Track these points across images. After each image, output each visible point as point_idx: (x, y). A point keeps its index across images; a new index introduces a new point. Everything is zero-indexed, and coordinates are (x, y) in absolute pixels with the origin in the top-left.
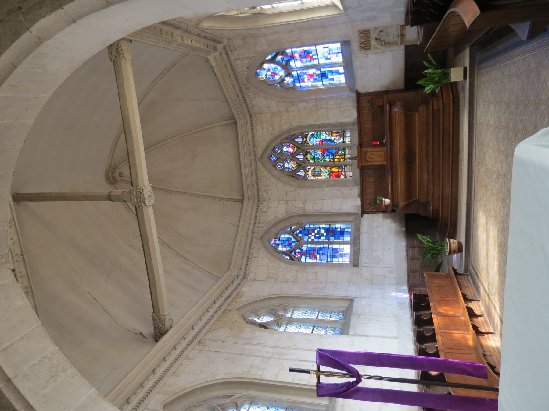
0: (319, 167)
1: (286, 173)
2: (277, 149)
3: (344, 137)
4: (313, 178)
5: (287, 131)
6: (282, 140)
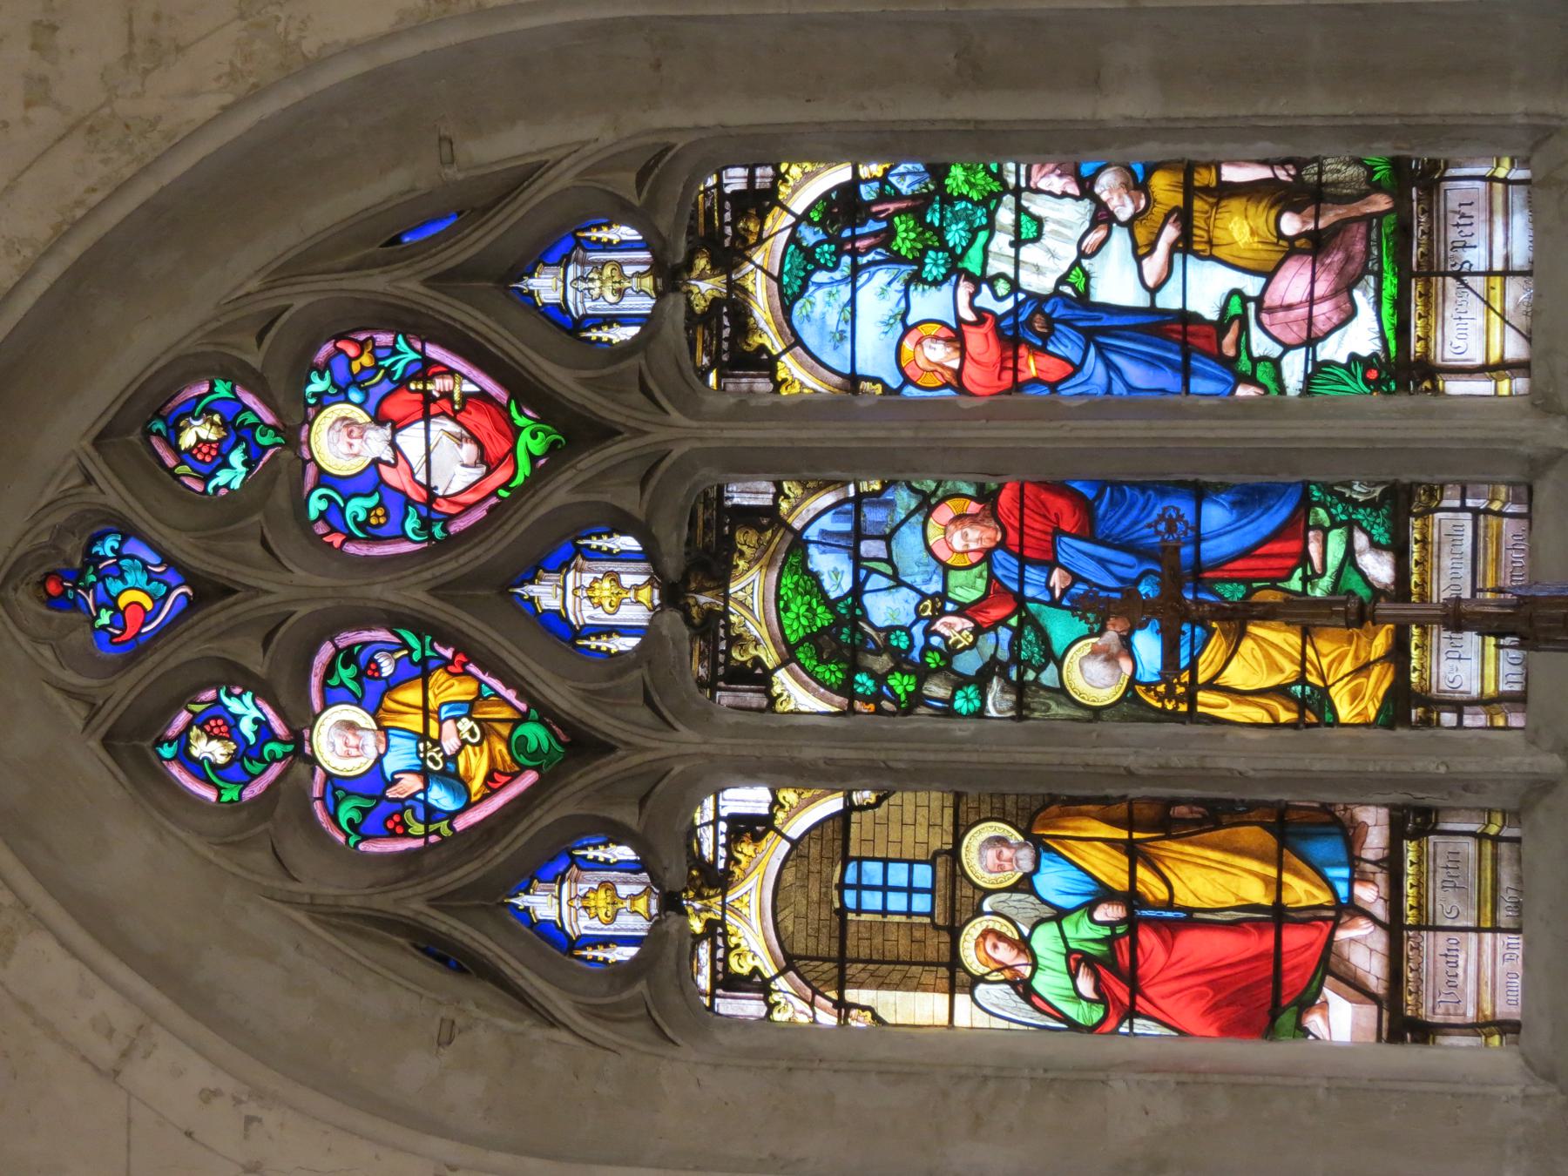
0: (917, 817)
1: (332, 886)
2: (195, 433)
3: (1420, 272)
4: (792, 1007)
5: (393, 100)
6: (288, 271)
